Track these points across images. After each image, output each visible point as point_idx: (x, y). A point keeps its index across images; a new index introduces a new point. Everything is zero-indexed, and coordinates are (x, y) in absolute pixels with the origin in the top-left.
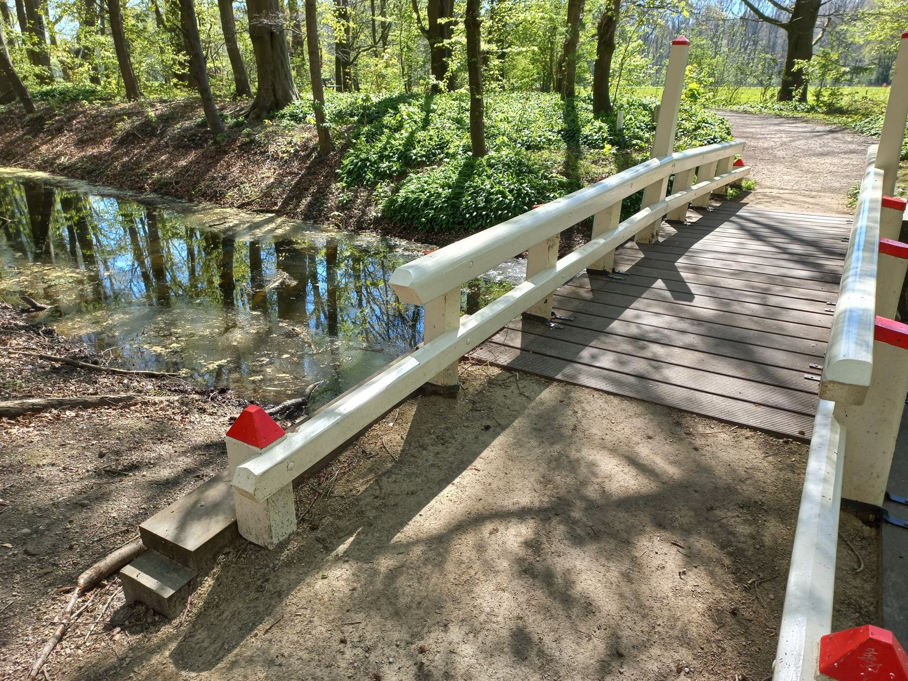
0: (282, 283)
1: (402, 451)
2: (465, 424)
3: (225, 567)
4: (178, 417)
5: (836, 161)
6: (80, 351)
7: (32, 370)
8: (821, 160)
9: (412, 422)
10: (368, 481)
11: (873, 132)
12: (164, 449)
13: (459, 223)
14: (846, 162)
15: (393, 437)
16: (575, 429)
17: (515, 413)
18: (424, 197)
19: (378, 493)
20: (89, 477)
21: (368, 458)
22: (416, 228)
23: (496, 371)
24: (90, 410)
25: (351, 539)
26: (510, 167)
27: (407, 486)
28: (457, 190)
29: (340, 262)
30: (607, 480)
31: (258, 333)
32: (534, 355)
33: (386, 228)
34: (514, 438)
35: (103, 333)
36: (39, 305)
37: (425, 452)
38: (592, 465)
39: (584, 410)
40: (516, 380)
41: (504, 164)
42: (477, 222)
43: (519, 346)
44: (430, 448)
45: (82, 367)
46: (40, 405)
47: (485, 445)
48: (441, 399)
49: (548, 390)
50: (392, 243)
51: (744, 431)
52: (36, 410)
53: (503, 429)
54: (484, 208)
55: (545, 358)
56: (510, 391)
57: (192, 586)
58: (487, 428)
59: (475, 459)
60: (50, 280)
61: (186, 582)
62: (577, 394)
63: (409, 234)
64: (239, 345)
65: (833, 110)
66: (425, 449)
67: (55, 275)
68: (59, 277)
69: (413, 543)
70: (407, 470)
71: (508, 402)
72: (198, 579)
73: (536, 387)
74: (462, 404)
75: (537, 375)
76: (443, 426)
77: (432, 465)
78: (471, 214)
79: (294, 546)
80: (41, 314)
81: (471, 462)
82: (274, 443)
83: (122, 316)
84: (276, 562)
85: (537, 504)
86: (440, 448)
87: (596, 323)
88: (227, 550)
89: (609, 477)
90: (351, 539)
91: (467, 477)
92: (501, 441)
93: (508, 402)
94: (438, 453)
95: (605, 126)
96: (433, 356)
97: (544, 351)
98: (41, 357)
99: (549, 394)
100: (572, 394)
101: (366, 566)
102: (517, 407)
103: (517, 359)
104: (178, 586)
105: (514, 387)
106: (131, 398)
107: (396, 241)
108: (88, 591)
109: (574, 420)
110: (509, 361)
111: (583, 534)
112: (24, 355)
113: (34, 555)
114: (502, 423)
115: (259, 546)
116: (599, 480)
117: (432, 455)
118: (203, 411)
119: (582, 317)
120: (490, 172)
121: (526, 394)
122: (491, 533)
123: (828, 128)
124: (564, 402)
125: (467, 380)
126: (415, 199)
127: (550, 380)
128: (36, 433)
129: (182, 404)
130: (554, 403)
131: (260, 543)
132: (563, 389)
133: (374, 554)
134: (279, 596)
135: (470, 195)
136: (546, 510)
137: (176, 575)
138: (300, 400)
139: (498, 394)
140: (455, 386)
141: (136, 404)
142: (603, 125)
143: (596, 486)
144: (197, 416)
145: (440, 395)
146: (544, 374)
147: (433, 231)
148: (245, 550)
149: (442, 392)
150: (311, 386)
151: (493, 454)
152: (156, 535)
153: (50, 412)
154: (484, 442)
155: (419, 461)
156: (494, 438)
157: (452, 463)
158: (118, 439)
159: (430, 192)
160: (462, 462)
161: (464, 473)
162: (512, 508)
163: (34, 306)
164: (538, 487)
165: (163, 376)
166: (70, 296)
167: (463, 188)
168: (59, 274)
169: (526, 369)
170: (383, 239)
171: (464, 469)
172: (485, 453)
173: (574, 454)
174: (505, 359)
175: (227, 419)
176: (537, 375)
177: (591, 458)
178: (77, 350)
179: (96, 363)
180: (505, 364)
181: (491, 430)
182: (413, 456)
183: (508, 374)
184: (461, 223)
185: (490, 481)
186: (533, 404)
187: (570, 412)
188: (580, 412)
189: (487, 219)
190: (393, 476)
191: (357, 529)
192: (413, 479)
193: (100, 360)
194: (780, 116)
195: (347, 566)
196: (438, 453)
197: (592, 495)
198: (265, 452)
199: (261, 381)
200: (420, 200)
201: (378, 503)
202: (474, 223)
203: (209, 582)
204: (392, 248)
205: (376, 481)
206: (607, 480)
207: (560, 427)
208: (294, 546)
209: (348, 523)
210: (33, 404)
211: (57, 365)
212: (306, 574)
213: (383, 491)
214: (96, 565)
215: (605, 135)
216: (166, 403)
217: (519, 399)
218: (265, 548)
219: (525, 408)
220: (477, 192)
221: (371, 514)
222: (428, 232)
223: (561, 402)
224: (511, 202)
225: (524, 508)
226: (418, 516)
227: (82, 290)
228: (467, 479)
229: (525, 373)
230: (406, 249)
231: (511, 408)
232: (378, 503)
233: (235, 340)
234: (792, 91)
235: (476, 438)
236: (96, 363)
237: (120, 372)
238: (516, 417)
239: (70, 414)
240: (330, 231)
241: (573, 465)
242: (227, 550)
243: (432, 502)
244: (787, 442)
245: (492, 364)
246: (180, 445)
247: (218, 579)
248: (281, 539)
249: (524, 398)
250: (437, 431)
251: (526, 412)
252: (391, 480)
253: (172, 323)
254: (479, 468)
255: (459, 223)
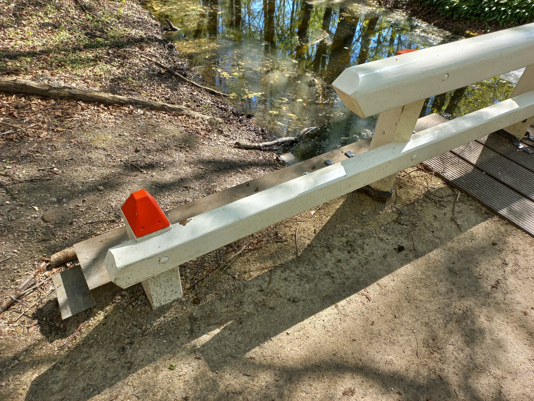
0: (322, 42)
1: (309, 246)
2: (381, 236)
4: (203, 133)
6: (181, 64)
7: (146, 71)
9: (332, 217)
10: (263, 269)
12: (180, 156)
15: (307, 230)
16: (495, 287)
17: (437, 241)
19: (264, 286)
20: (119, 166)
21: (277, 242)
22: (439, 13)
23: (438, 183)
24: (153, 112)
25: (217, 331)
27: (293, 290)
29: (376, 32)
30: (509, 377)
31: (290, 77)
33: (416, 10)
34: (423, 273)
35: (200, 54)
36: (174, 27)
37: (328, 255)
38: (499, 345)
39: (516, 264)
40: (455, 202)
42: (493, 16)
43: (474, 161)
44: (336, 252)
45: (176, 76)
46: (124, 101)
47: (389, 270)
48: (369, 200)
49: (484, 224)
50: (415, 23)
52: (121, 104)
53: (417, 257)
55: (497, 184)
56: (443, 212)
57: (89, 314)
58: (401, 249)
59: (372, 282)
60: (188, 11)
61: (84, 309)
62: (515, 240)
63: (431, 18)
64: (274, 84)
66: (330, 251)
67: (191, 8)
68: (193, 10)
69: (264, 366)
70: (303, 269)
71: (436, 224)
72: (95, 310)
73: (473, 217)
74: (388, 209)
75: (479, 202)
76: (358, 231)
77: (328, 274)
79: (170, 315)
80: (174, 33)
81: (366, 284)
82: (154, 234)
83: (215, 45)
84: (149, 326)
85: (412, 375)
86: (344, 255)
89: (515, 374)
90: (217, 331)
91: (352, 304)
92: (407, 270)
93: (436, 224)
94: (339, 261)
96: (365, 168)
98: (156, 64)
99: (482, 229)
100: (510, 239)
101: (210, 374)
102: (442, 235)
103: (467, 176)
104: (78, 310)
105: (449, 208)
106: (181, 110)
107: (417, 22)
108: (56, 267)
109: (500, 273)
110: (456, 176)
112: (148, 59)
113: (46, 222)
114: (419, 248)
116: (499, 372)
117: (334, 260)
118: (221, 132)
121: (459, 222)
122: (344, 394)
124: (495, 246)
125: (405, 185)
127: (491, 212)
128: (114, 120)
129: (210, 123)
130: (485, 244)
132: (502, 229)
133: (225, 362)
134: (129, 369)
136: (419, 387)
138: (293, 138)
139: (430, 211)
140: (388, 192)
141: (183, 115)
143: (492, 380)
144: (215, 135)
145: (370, 195)
147: (452, 18)
149: (373, 194)
150: (306, 129)
151: (392, 284)
153: (129, 108)
154: (389, 266)
155: (318, 263)
156: (402, 265)
157: (348, 279)
158: (155, 140)
160: (358, 282)
161: (352, 297)
162: (384, 368)
163: (171, 27)
164: (423, 351)
165: (220, 95)
166: (194, 24)
168: (194, 8)
169: (471, 191)
170: (409, 20)
171: (356, 291)
172: (385, 280)
173: (482, 321)
174: (452, 173)
175: (235, 142)
176: (479, 202)
177: (502, 335)
178: (180, 63)
179: (185, 75)
181: (404, 253)
182: (315, 255)
183: (449, 191)
184: (478, 15)
185: (374, 318)
186: (462, 236)
187: (499, 262)
188: (511, 265)
189: (503, 14)
190: (288, 271)
191: (227, 321)
192: (303, 282)
193: (188, 73)
195: (195, 364)
196: (339, 261)
197: (483, 391)
198: (141, 241)
199: (276, 115)
201: (260, 298)
202: (490, 17)
203: (100, 316)
204: (413, 28)
205: (271, 271)
206: (509, 377)
207: (480, 277)
208: (170, 315)
209: (225, 310)
210: (120, 100)
211: (163, 71)
212: (161, 354)
213: (271, 286)
214: (66, 250)
216: (200, 120)
217: (449, 226)
219: (451, 239)
221: (248, 308)
222: (447, 19)
223: (494, 244)
225: (395, 373)
226: (284, 333)
227: (202, 21)
228: (353, 305)
229: (468, 195)
230: (424, 31)
231: (436, 233)
232: (260, 298)
233: (273, 80)
235: (385, 257)
236: (185, 75)
237: (196, 86)
238: (436, 247)
239: (140, 111)
240: (373, 6)
241: (472, 336)
243: (306, 321)
245: (437, 175)
246: (193, 156)
248: (163, 304)
249: (454, 226)
250: (351, 235)
251: (449, 244)
252: (284, 275)
253: (241, 57)
254: (371, 296)
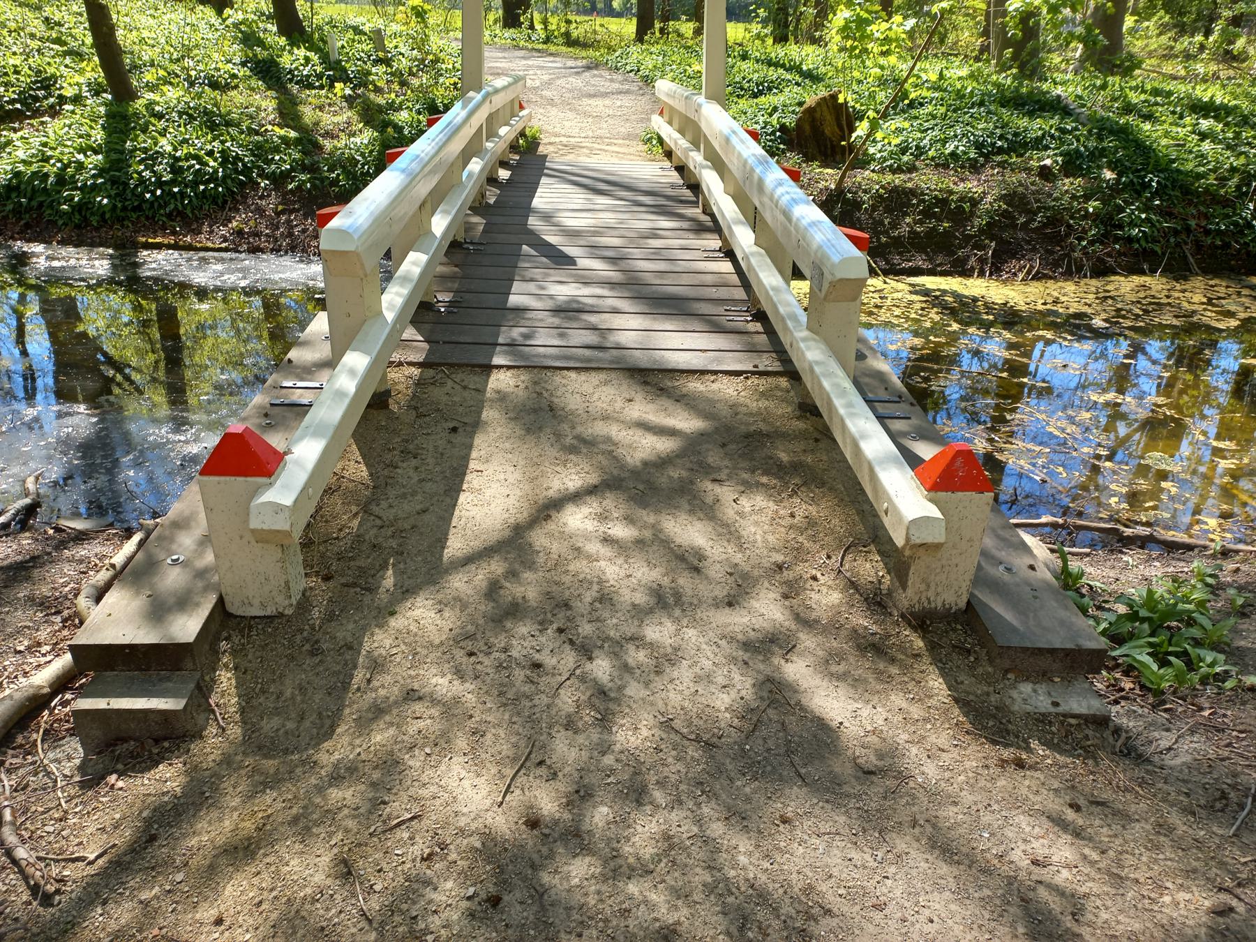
3: (234, 653)
5: (607, 102)
8: (592, 102)
11: (628, 68)
13: (135, 209)
14: (619, 103)
18: (52, 169)
26: (191, 116)
28: (114, 156)
32: (447, 346)
41: (180, 114)
51: (707, 377)
54: (173, 182)
65: (570, 42)
75: (467, 365)
78: (153, 193)
87: (490, 300)
88: (225, 634)
95: (315, 57)
97: (454, 338)
111: (684, 474)
115: (268, 617)
119: (467, 296)
120: (161, 124)
123: (579, 63)
126: (34, 173)
131: (269, 611)
135: (140, 162)
137: (170, 685)
142: (311, 54)
146: (475, 362)
148: (250, 627)
152: (110, 645)
159: (60, 161)
167: (122, 152)
172: (474, 454)
176: (467, 365)
180: (421, 360)
184: (138, 208)
189: (183, 198)
194: (517, 47)
200: (46, 175)
215: (319, 69)
218: (281, 615)
220: (152, 158)
224: (216, 171)
229: (451, 365)
234: (519, 15)
242: (225, 634)
244: (747, 378)
247: (236, 668)
255: (135, 209)
